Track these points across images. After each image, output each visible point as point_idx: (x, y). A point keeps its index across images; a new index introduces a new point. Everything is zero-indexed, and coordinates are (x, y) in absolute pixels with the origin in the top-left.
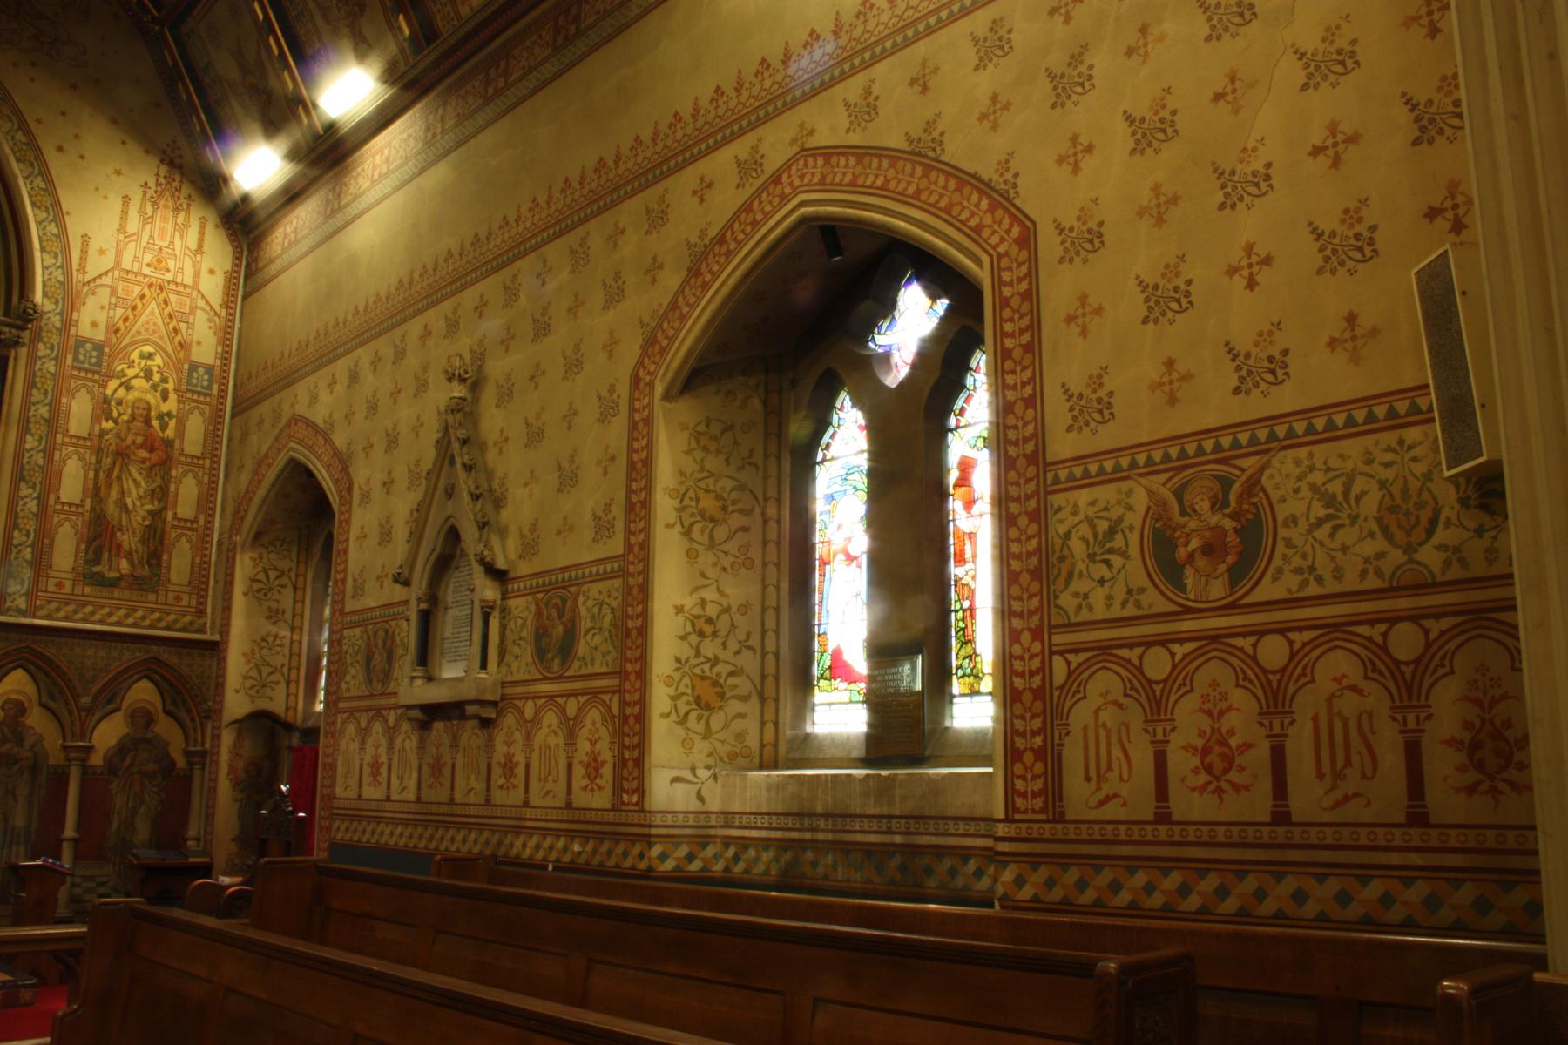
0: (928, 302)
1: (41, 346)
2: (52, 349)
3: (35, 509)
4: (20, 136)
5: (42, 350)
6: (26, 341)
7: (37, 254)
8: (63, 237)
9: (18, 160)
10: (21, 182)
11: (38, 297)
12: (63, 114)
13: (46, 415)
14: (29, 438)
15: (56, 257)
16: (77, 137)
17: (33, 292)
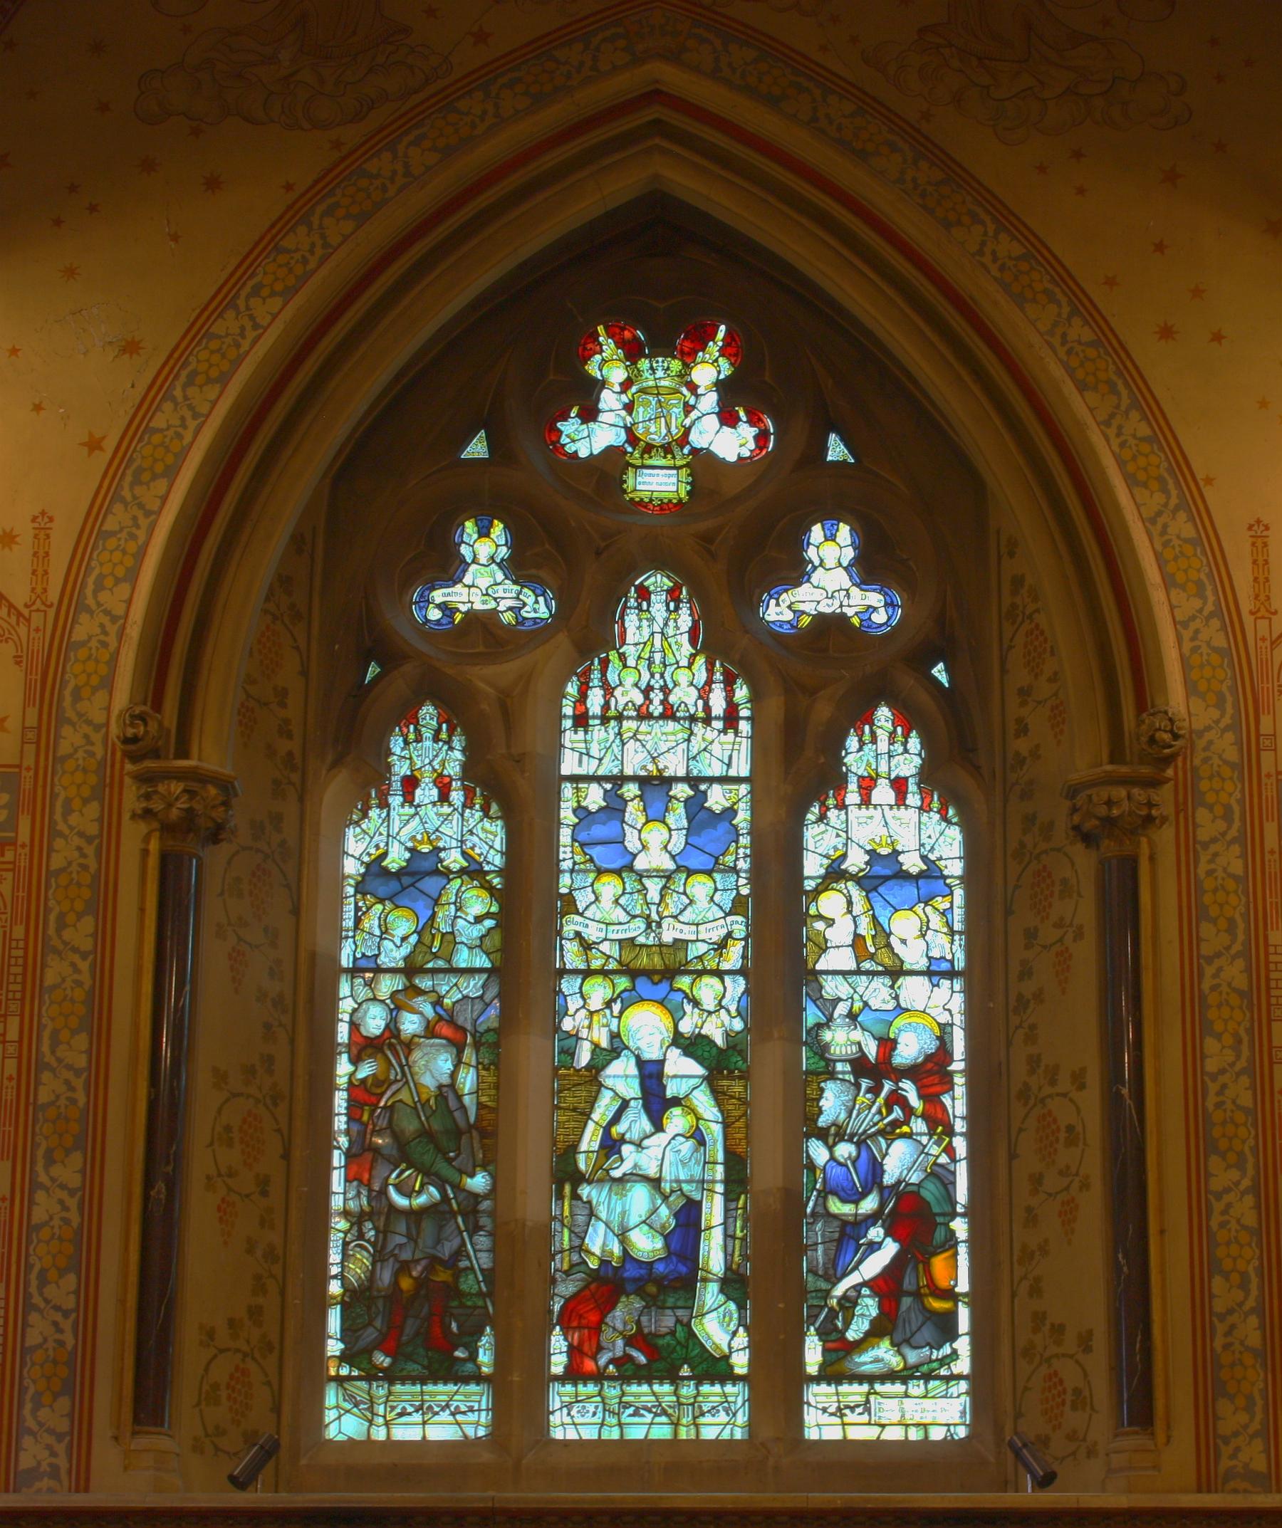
0: (717, 425)
1: (1202, 815)
2: (1227, 816)
3: (1250, 1220)
4: (1080, 331)
5: (1207, 824)
6: (1169, 810)
7: (1158, 596)
8: (1208, 540)
9: (1082, 387)
10: (1096, 437)
11: (1176, 698)
12: (1160, 247)
13: (1241, 982)
14: (1211, 1045)
15: (1201, 594)
16: (1197, 292)
17: (1164, 689)
